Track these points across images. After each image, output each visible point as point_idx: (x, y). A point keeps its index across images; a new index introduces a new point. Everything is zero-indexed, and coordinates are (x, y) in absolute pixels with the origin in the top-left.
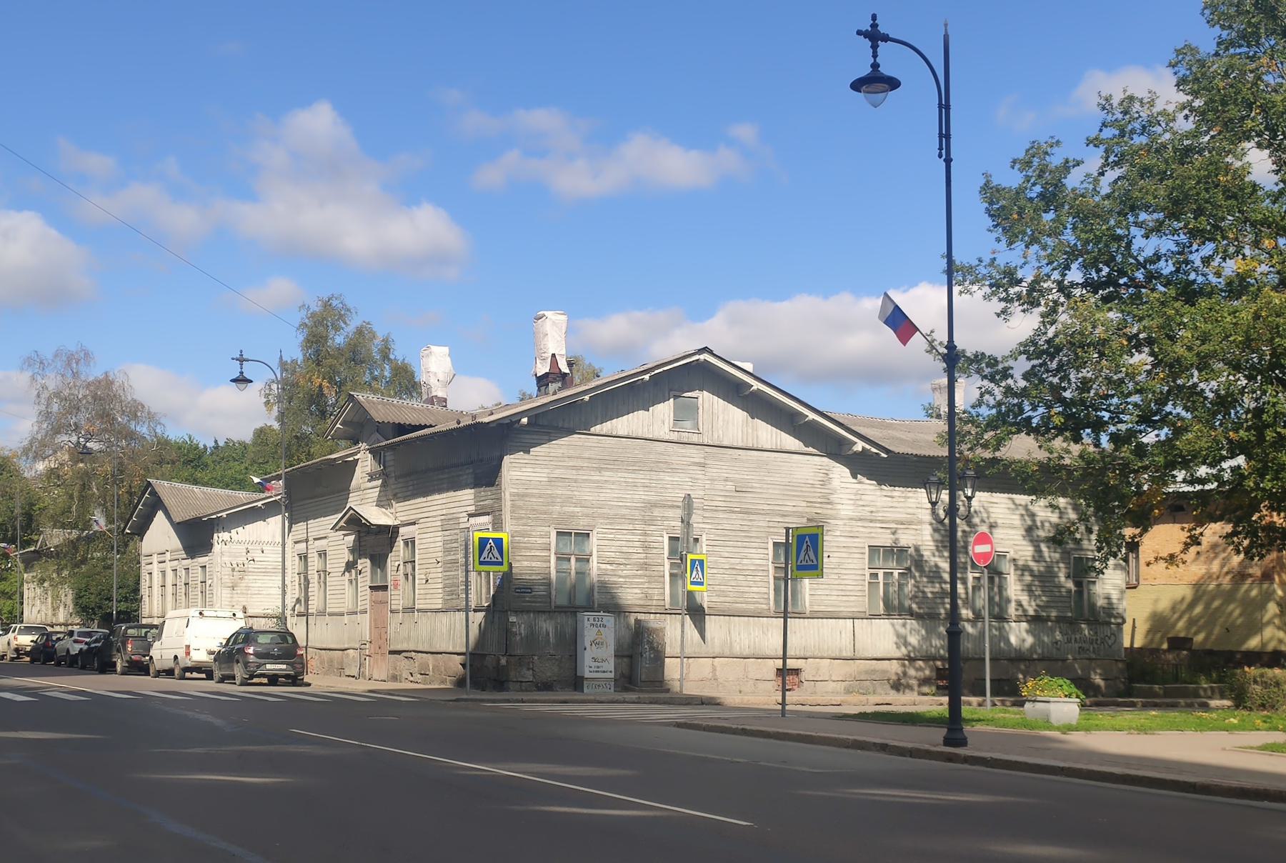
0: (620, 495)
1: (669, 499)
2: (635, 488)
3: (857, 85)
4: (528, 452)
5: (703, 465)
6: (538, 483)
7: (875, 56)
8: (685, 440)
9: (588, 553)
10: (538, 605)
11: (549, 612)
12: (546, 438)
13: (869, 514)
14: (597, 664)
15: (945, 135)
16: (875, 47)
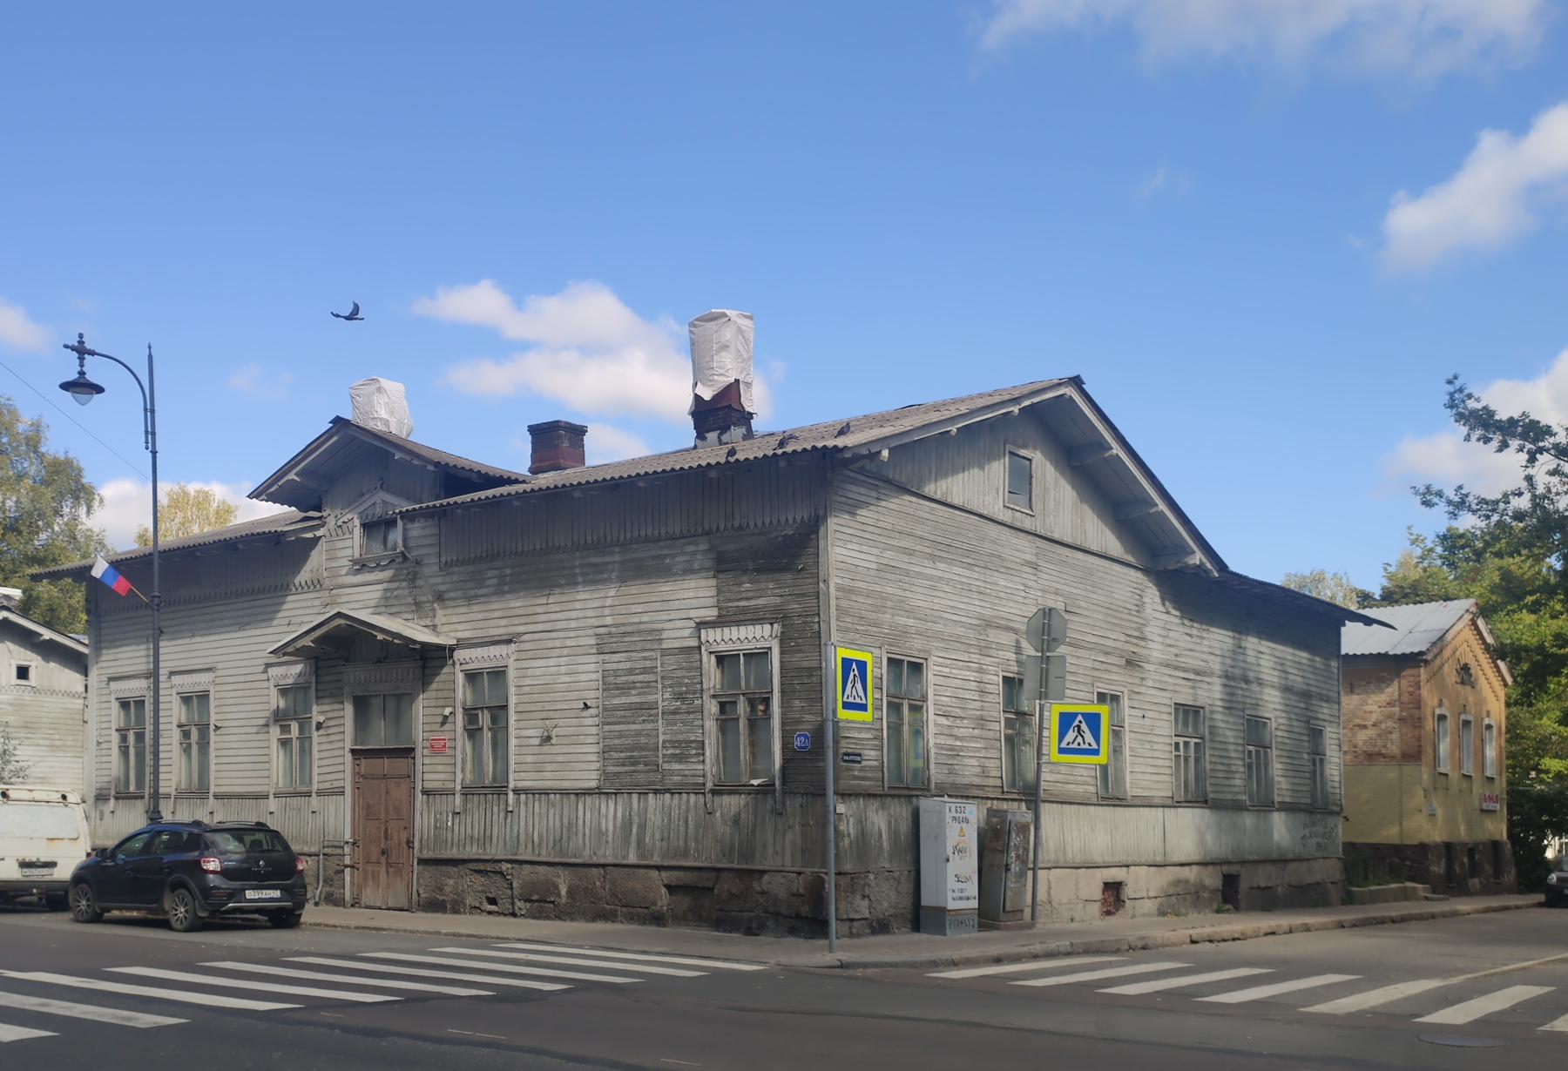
0: (955, 604)
1: (1004, 615)
2: (969, 594)
3: (66, 386)
4: (853, 514)
5: (1035, 567)
6: (865, 571)
7: (82, 365)
8: (1018, 525)
9: (918, 696)
10: (868, 783)
11: (881, 796)
12: (874, 494)
13: (1174, 658)
14: (960, 885)
15: (151, 433)
16: (81, 359)
